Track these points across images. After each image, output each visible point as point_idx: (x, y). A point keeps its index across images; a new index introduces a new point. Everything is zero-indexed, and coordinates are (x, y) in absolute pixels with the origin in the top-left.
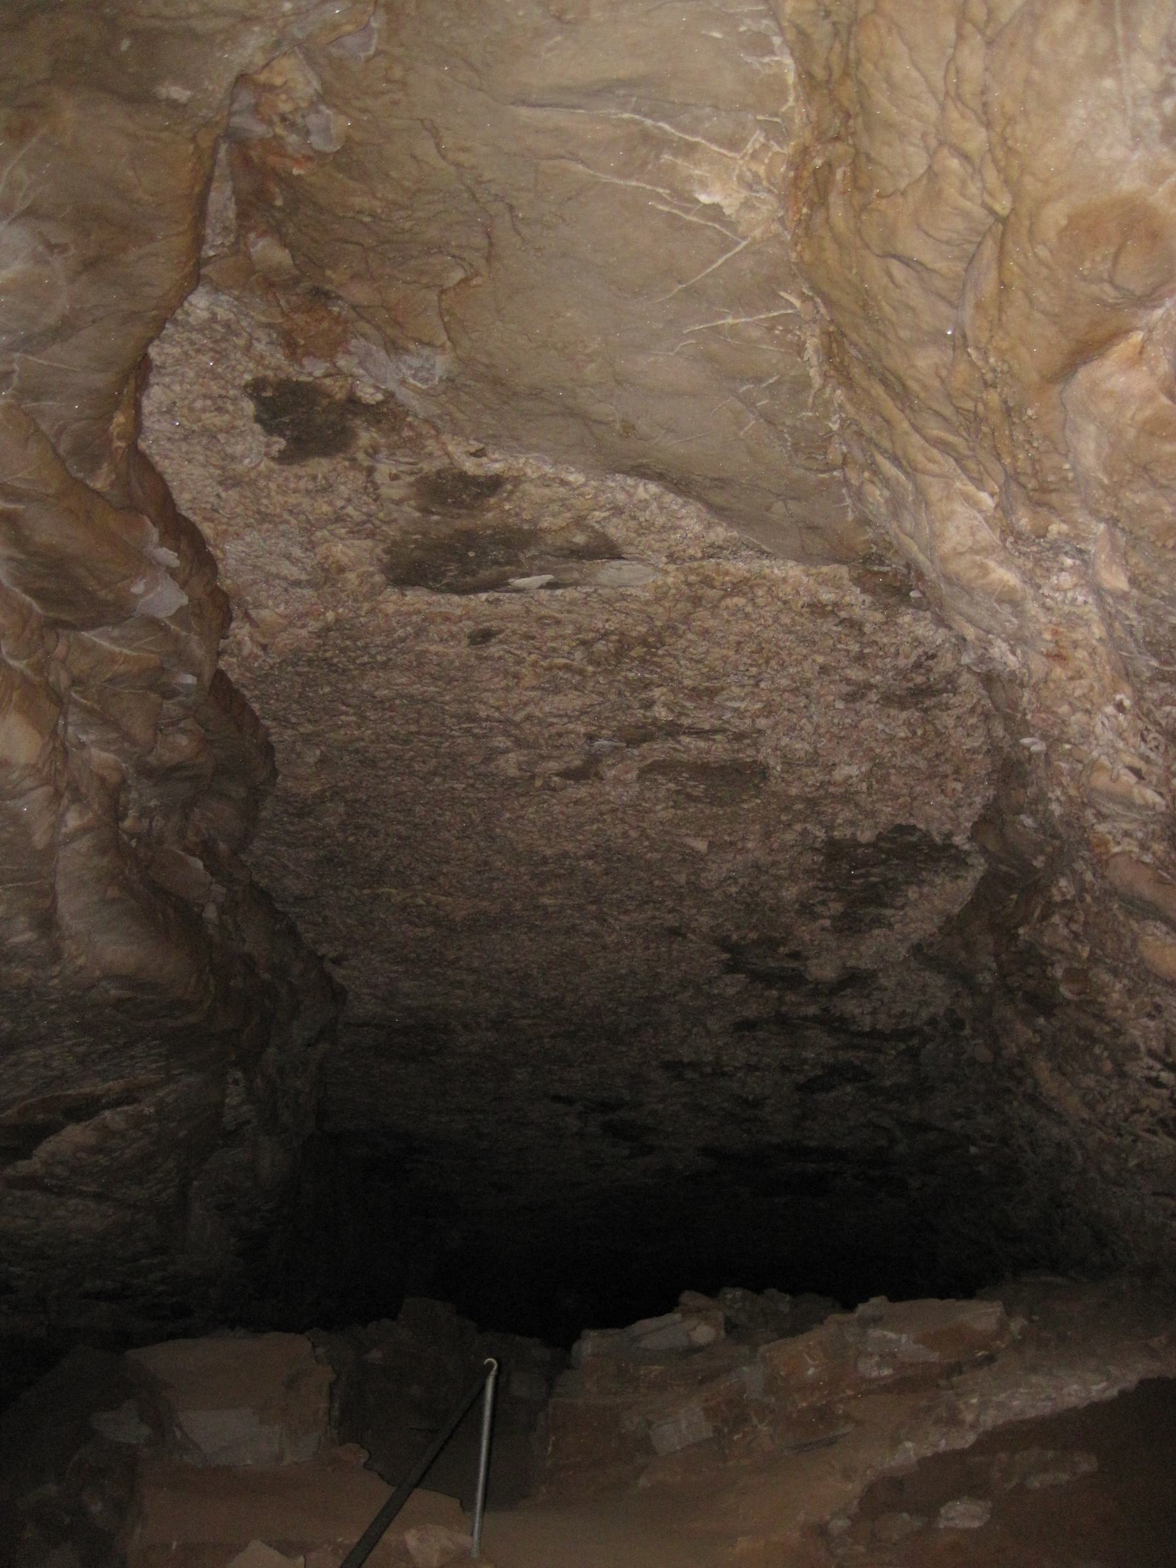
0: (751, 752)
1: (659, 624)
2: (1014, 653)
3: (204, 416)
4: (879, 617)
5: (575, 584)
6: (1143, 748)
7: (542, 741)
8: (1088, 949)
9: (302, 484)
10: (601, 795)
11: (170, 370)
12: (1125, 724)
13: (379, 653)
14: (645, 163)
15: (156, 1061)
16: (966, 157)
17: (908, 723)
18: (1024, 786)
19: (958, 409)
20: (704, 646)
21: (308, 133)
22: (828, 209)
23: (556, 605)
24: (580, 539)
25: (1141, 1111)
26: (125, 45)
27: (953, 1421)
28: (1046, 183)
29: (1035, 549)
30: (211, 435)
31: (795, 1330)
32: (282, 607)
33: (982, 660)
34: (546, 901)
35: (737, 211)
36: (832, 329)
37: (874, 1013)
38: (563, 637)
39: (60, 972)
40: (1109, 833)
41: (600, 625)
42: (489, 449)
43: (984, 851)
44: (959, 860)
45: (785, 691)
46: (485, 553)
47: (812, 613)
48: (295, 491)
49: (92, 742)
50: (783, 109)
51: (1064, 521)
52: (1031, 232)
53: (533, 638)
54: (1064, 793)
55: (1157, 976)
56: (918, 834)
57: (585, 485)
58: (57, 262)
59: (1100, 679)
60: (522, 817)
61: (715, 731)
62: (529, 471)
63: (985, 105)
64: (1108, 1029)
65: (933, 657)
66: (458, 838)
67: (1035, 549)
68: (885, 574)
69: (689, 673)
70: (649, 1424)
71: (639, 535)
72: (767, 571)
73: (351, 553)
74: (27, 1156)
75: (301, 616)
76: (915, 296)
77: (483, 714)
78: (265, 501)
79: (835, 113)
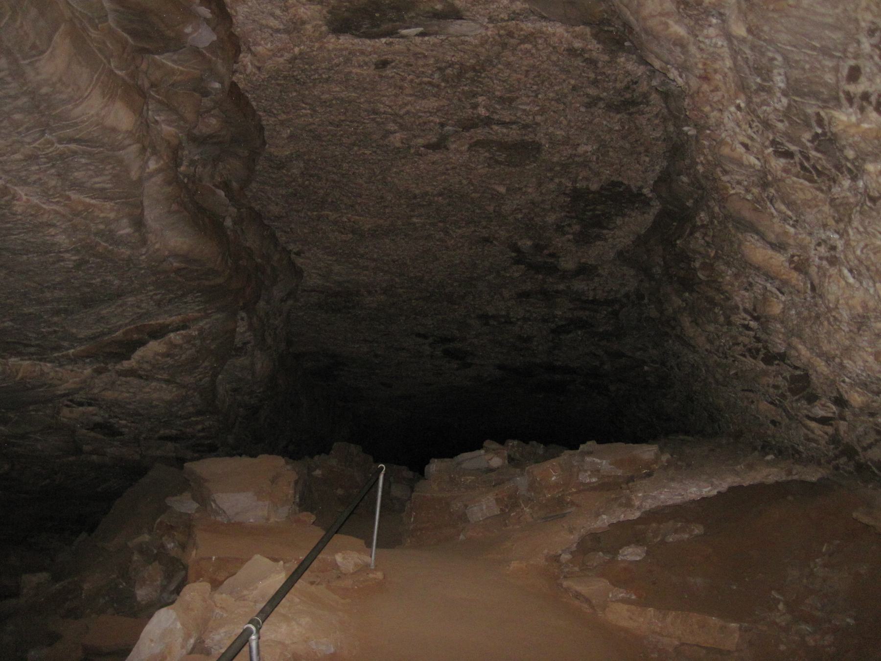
0: (532, 136)
1: (482, 58)
2: (681, 76)
4: (607, 58)
5: (436, 33)
6: (750, 131)
7: (415, 127)
8: (714, 252)
12: (741, 117)
13: (324, 73)
15: (198, 305)
20: (507, 72)
23: (424, 46)
25: (738, 344)
27: (629, 505)
29: (695, 12)
31: (545, 458)
32: (269, 45)
33: (663, 83)
34: (414, 220)
39: (146, 252)
41: (449, 58)
45: (552, 100)
47: (569, 54)
49: (163, 121)
53: (411, 65)
55: (751, 265)
59: (728, 91)
61: (514, 123)
65: (636, 83)
66: (366, 183)
67: (695, 12)
68: (612, 32)
70: (466, 506)
71: (473, 5)
72: (544, 29)
74: (129, 359)
75: (280, 50)
77: (382, 110)
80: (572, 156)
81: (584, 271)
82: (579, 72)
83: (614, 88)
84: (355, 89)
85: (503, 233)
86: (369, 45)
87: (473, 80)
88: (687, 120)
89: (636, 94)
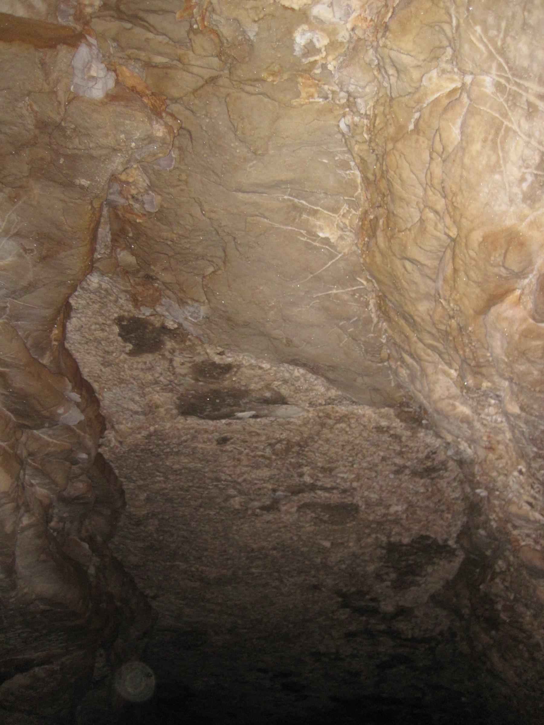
0: (350, 499)
2: (470, 447)
3: (95, 333)
4: (409, 433)
5: (266, 416)
6: (532, 492)
7: (251, 492)
9: (140, 366)
10: (280, 519)
11: (80, 311)
12: (523, 481)
13: (175, 447)
14: (295, 219)
15: (61, 643)
16: (436, 212)
17: (424, 485)
18: (480, 515)
19: (439, 330)
20: (326, 447)
21: (144, 204)
22: (376, 238)
23: (257, 426)
24: (268, 394)
26: (62, 161)
28: (472, 222)
29: (476, 395)
30: (98, 341)
34: (253, 570)
35: (337, 241)
36: (380, 294)
37: (413, 629)
38: (261, 442)
40: (519, 535)
41: (278, 436)
42: (226, 351)
43: (462, 547)
44: (452, 553)
45: (365, 469)
46: (224, 401)
47: (377, 431)
48: (136, 369)
49: (37, 484)
50: (356, 194)
51: (489, 381)
52: (466, 245)
53: (247, 442)
54: (497, 516)
56: (431, 540)
57: (270, 369)
58: (28, 257)
59: (510, 459)
60: (242, 529)
61: (333, 488)
62: (244, 362)
63: (443, 188)
64: (525, 635)
65: (435, 453)
67: (476, 395)
68: (411, 412)
69: (320, 460)
71: (296, 393)
72: (356, 411)
73: (162, 399)
75: (139, 428)
76: (417, 277)
78: (122, 373)
79: (378, 194)
80: (384, 515)
81: (402, 612)
82: (386, 446)
83: (417, 458)
84: (201, 460)
85: (329, 582)
86: (212, 426)
87: (298, 453)
88: (478, 485)
89: (436, 463)
